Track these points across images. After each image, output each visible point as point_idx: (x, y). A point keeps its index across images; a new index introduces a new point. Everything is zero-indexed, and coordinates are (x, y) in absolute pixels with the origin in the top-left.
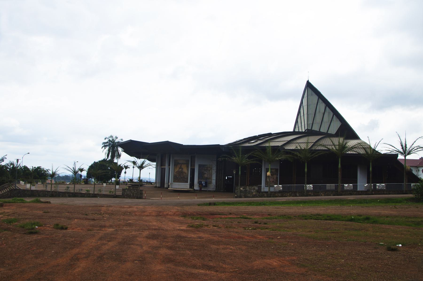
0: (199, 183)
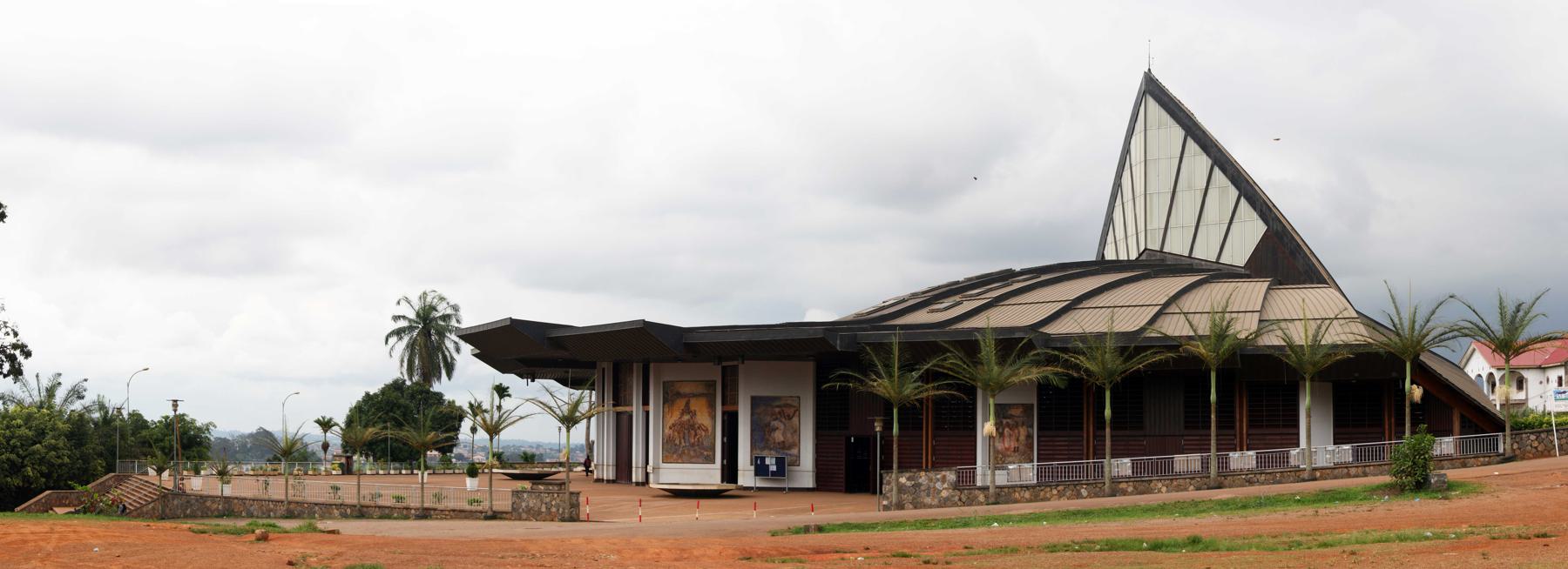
0: (756, 461)
